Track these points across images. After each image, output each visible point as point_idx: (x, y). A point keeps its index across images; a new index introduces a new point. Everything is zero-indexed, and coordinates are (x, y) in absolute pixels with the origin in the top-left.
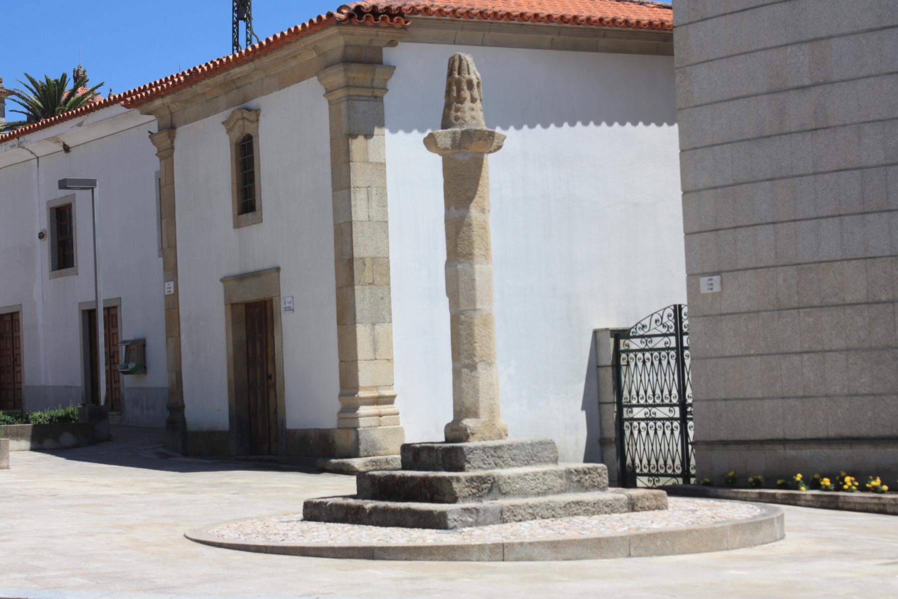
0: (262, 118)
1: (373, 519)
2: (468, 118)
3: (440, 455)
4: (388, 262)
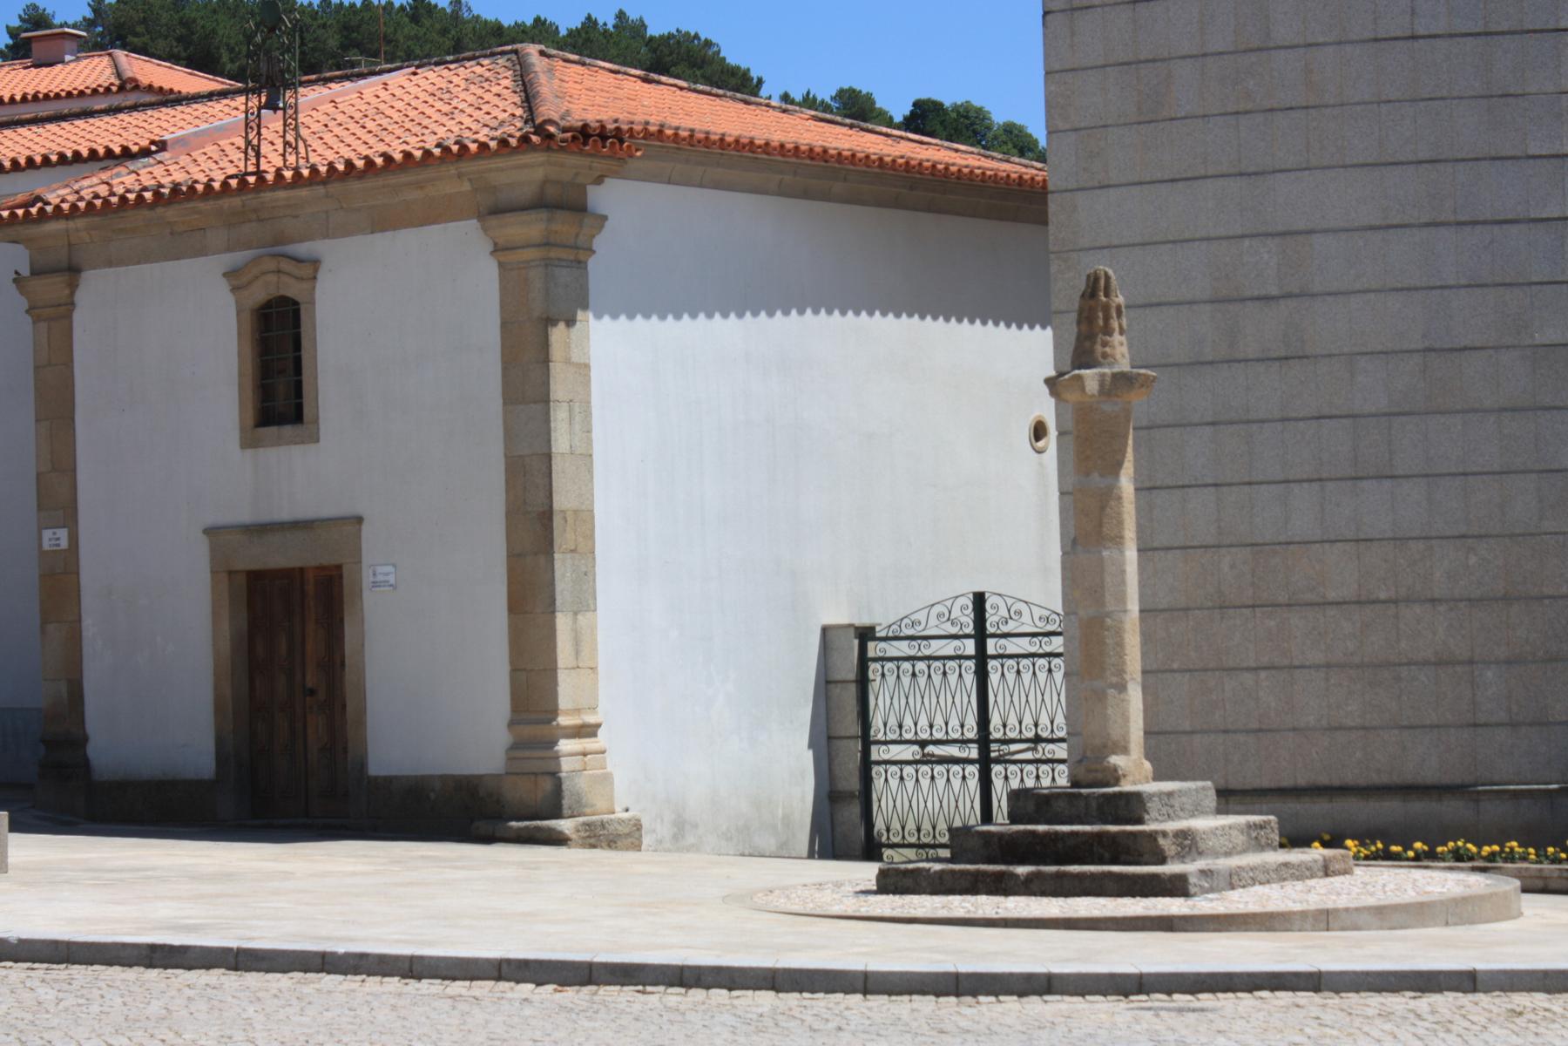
4: (593, 517)
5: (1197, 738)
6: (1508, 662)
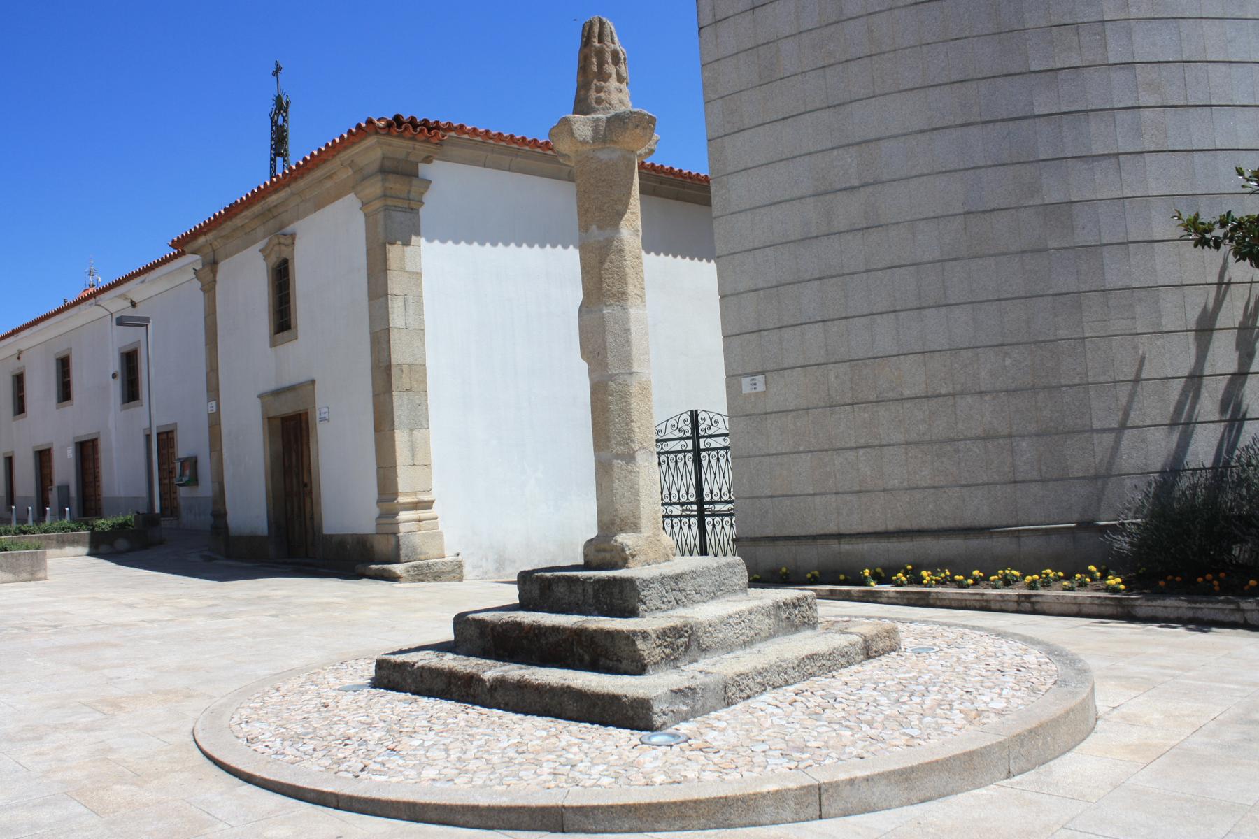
0: (297, 242)
1: (499, 696)
2: (614, 102)
3: (590, 591)
5: (818, 499)
6: (1037, 435)
